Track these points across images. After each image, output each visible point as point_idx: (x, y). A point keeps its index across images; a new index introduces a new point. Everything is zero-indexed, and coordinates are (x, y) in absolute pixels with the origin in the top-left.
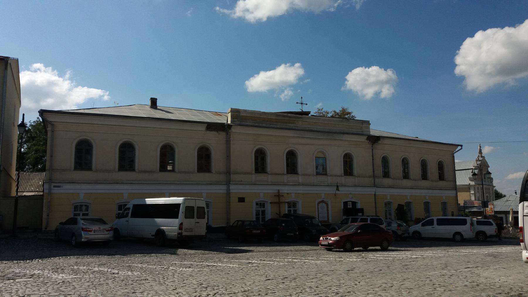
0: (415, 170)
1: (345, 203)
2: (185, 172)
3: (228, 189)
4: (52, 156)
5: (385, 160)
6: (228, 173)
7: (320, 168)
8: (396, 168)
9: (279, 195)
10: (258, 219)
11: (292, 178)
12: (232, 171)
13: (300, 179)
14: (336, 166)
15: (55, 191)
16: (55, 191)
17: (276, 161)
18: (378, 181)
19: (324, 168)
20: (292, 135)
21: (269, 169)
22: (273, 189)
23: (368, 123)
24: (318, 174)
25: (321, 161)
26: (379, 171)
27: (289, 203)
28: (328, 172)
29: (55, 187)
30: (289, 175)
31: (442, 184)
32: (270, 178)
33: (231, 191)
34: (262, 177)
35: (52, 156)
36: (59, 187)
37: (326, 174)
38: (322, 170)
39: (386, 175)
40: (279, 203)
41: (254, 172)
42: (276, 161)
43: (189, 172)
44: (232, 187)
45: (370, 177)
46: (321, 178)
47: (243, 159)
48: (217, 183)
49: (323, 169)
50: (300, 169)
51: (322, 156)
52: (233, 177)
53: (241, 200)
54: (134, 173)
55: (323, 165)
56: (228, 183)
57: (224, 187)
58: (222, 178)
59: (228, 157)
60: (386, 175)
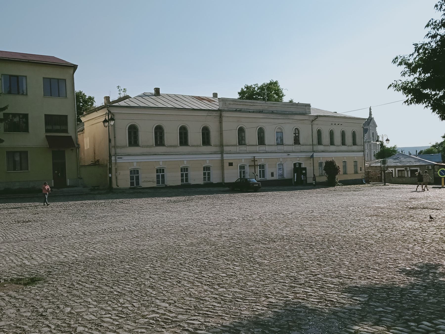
0: (338, 139)
1: (295, 164)
2: (171, 146)
3: (222, 157)
4: (115, 137)
5: (319, 133)
6: (222, 145)
7: (279, 140)
8: (326, 139)
9: (254, 160)
10: (132, 184)
11: (262, 148)
12: (224, 144)
13: (267, 148)
14: (289, 138)
15: (119, 161)
16: (119, 161)
17: (251, 137)
18: (315, 148)
19: (282, 140)
20: (282, 118)
21: (189, 143)
22: (250, 156)
23: (309, 105)
24: (278, 144)
25: (279, 135)
26: (316, 141)
27: (260, 165)
28: (284, 142)
29: (118, 158)
30: (240, 146)
31: (355, 148)
32: (249, 149)
33: (224, 158)
34: (243, 148)
35: (115, 137)
36: (121, 158)
37: (283, 144)
38: (280, 142)
39: (320, 143)
40: (255, 166)
41: (238, 144)
42: (251, 137)
43: (198, 146)
44: (225, 155)
45: (310, 145)
46: (280, 147)
47: (231, 137)
48: (215, 153)
49: (281, 140)
50: (267, 142)
51: (279, 131)
52: (226, 149)
53: (231, 164)
54: (188, 147)
55: (281, 138)
56: (222, 153)
57: (220, 156)
58: (217, 149)
59: (221, 134)
60: (320, 143)
